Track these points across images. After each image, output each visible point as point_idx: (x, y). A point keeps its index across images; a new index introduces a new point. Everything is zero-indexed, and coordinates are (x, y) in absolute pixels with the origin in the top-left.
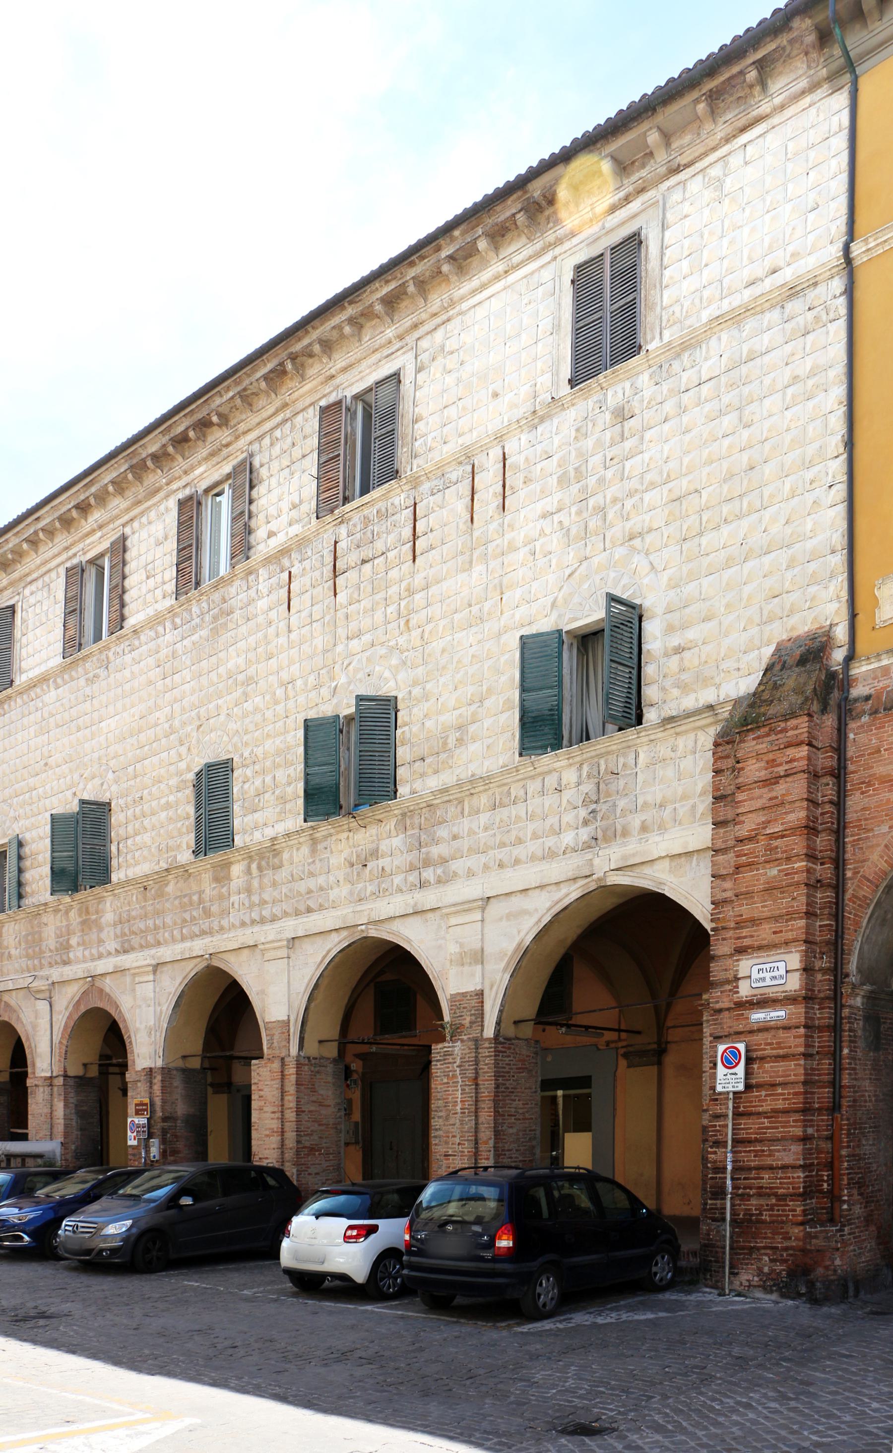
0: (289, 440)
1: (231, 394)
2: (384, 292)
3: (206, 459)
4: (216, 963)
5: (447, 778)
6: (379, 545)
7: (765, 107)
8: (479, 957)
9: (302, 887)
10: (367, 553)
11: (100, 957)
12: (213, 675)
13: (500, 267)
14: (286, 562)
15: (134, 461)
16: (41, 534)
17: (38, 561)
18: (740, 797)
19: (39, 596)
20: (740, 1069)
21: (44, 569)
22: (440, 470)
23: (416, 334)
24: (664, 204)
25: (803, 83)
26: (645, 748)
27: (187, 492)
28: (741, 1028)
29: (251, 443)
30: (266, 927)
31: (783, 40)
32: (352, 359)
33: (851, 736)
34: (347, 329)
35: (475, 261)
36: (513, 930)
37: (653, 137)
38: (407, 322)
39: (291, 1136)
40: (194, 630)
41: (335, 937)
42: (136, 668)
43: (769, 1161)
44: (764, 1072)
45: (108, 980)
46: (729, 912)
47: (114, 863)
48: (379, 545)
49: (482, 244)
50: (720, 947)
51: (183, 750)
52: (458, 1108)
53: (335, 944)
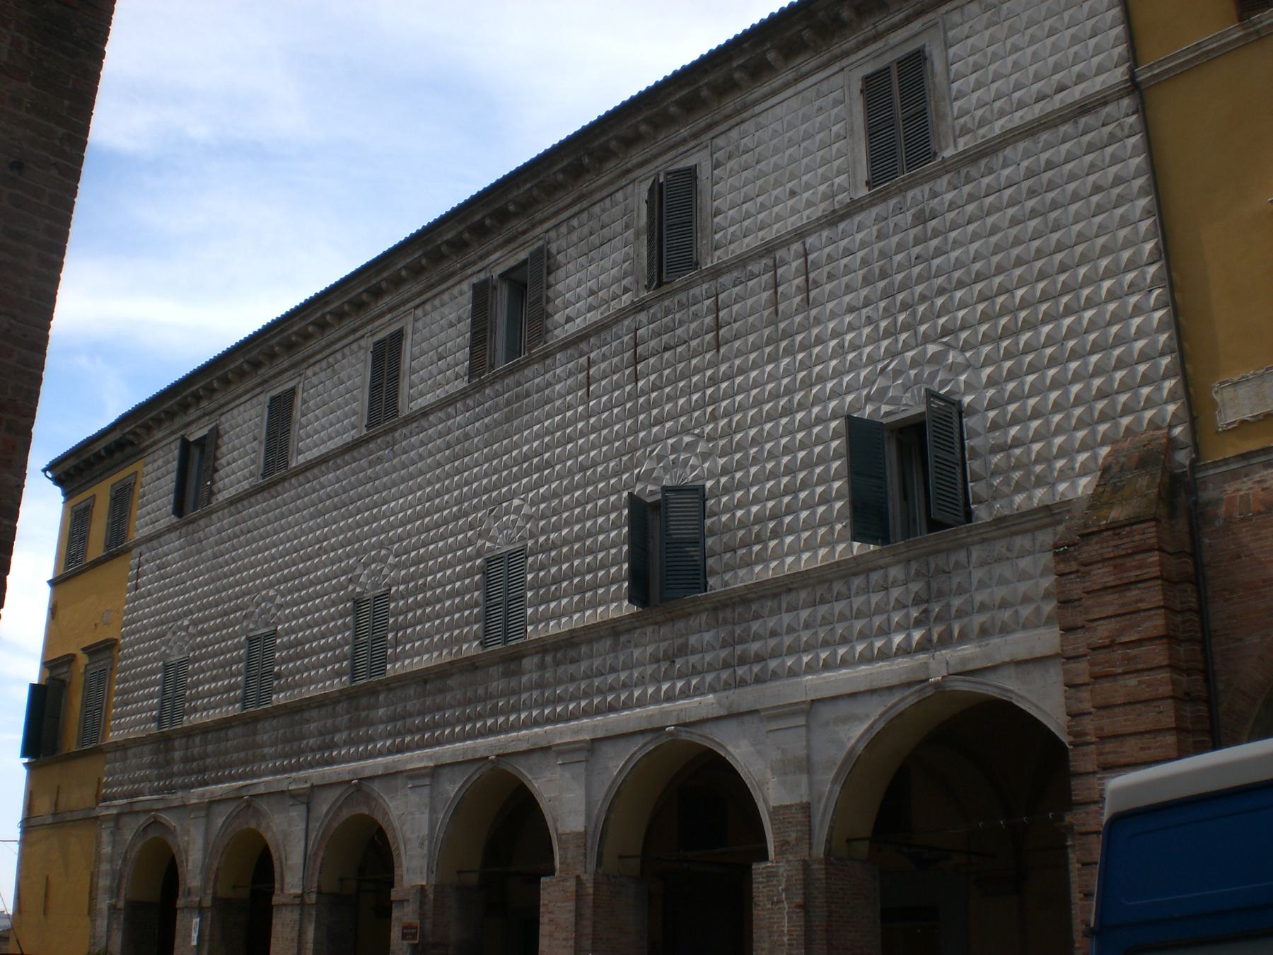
0: (586, 230)
1: (529, 185)
2: (677, 96)
3: (501, 246)
8: (807, 766)
13: (789, 76)
15: (429, 248)
16: (328, 317)
17: (323, 343)
19: (322, 376)
21: (328, 351)
23: (711, 134)
24: (944, 26)
26: (978, 547)
27: (482, 276)
29: (547, 231)
32: (648, 155)
33: (1206, 541)
38: (702, 123)
41: (641, 741)
46: (1088, 724)
50: (1083, 761)
52: (785, 939)
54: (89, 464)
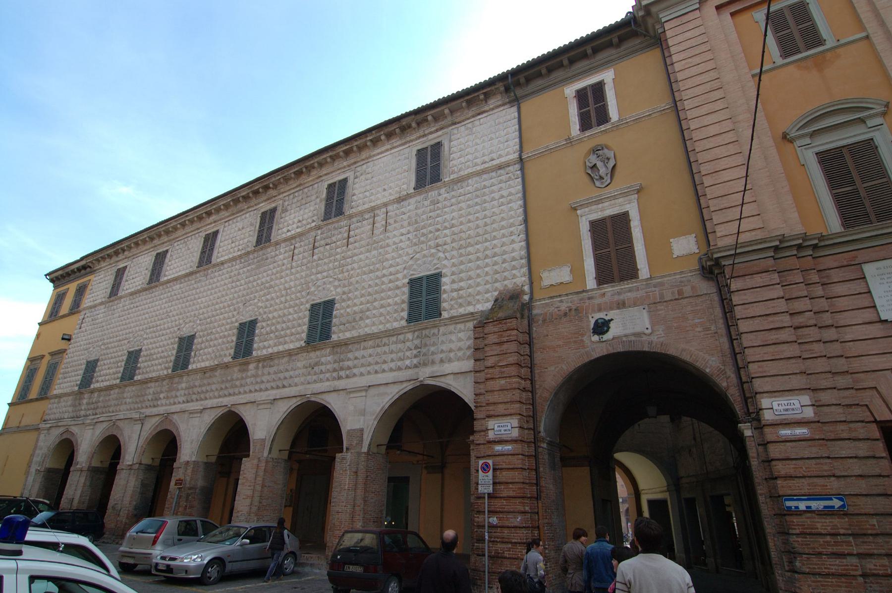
3: (265, 201)
4: (233, 409)
5: (355, 333)
6: (334, 239)
7: (486, 108)
9: (282, 375)
10: (328, 241)
11: (175, 404)
12: (255, 283)
13: (389, 147)
14: (293, 241)
18: (487, 349)
20: (490, 473)
22: (362, 213)
25: (500, 103)
28: (490, 453)
30: (262, 393)
31: (493, 88)
34: (329, 160)
35: (380, 143)
36: (380, 401)
37: (447, 111)
38: (352, 161)
39: (257, 499)
40: (249, 265)
41: (295, 400)
42: (219, 278)
43: (507, 523)
44: (504, 476)
45: (175, 416)
46: (481, 399)
47: (192, 360)
48: (334, 239)
49: (383, 137)
50: (478, 415)
51: (235, 313)
53: (294, 403)
54: (68, 274)
